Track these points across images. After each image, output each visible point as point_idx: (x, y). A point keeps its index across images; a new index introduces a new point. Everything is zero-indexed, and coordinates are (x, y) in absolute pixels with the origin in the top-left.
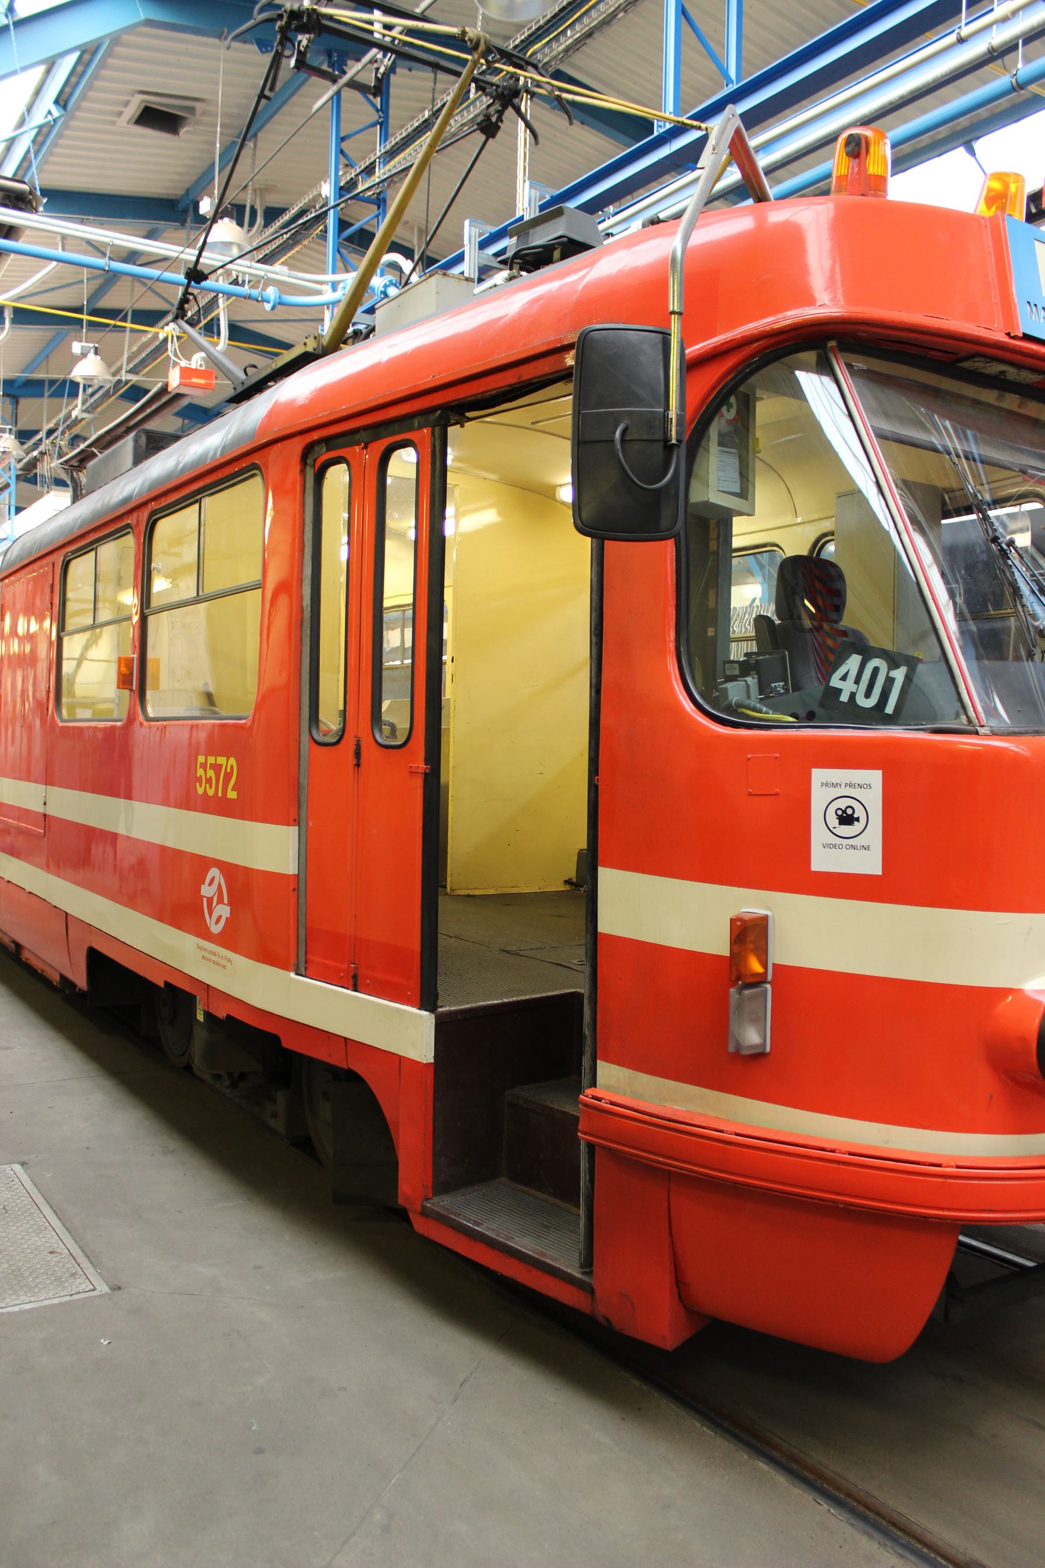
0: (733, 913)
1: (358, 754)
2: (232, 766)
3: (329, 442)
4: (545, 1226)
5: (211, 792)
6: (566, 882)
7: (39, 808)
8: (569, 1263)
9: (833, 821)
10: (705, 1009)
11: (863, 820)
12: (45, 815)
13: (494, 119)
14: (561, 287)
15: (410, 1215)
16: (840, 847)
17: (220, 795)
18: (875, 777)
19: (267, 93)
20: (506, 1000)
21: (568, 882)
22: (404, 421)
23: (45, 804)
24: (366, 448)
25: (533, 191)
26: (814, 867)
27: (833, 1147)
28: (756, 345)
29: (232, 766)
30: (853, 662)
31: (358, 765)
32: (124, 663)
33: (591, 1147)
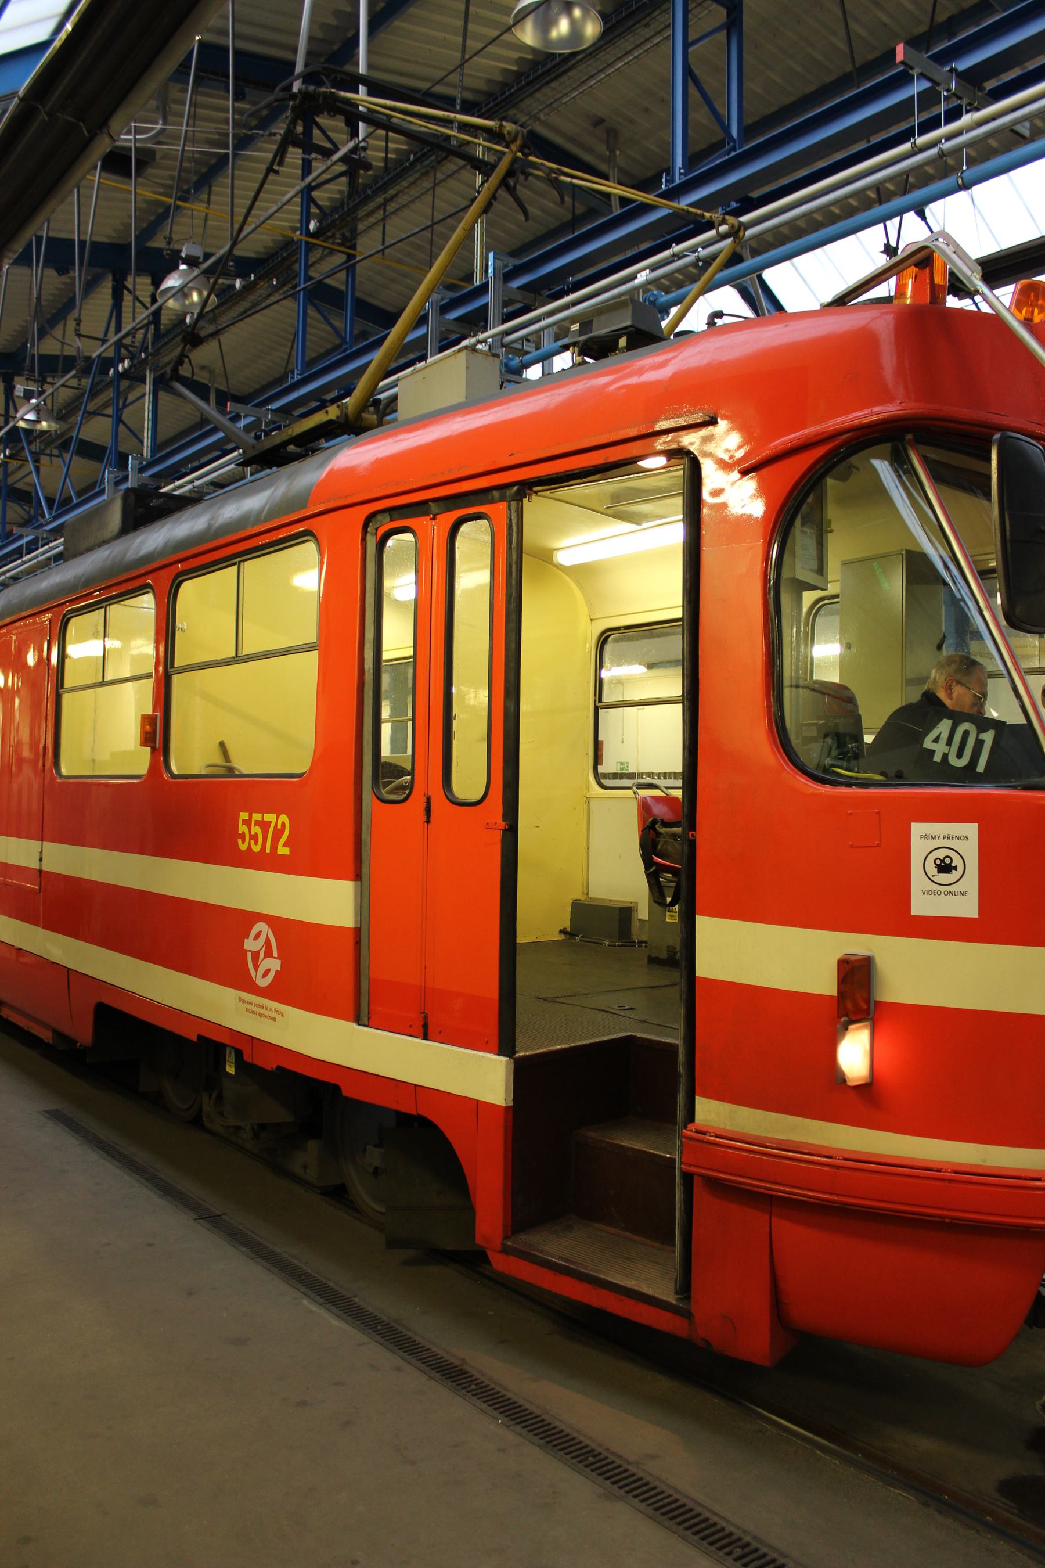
0: (839, 955)
1: (428, 811)
2: (283, 824)
3: (393, 512)
4: (627, 1259)
5: (256, 848)
6: (561, 931)
7: (36, 865)
8: (665, 1290)
9: (932, 870)
10: (784, 1046)
11: (960, 868)
12: (41, 871)
15: (489, 1253)
16: (939, 893)
17: (268, 850)
18: (971, 830)
20: (572, 1045)
21: (563, 932)
23: (41, 860)
24: (434, 519)
25: (498, 262)
26: (915, 912)
27: (939, 1167)
28: (844, 437)
29: (283, 824)
30: (944, 727)
31: (428, 822)
32: (148, 720)
33: (688, 1178)
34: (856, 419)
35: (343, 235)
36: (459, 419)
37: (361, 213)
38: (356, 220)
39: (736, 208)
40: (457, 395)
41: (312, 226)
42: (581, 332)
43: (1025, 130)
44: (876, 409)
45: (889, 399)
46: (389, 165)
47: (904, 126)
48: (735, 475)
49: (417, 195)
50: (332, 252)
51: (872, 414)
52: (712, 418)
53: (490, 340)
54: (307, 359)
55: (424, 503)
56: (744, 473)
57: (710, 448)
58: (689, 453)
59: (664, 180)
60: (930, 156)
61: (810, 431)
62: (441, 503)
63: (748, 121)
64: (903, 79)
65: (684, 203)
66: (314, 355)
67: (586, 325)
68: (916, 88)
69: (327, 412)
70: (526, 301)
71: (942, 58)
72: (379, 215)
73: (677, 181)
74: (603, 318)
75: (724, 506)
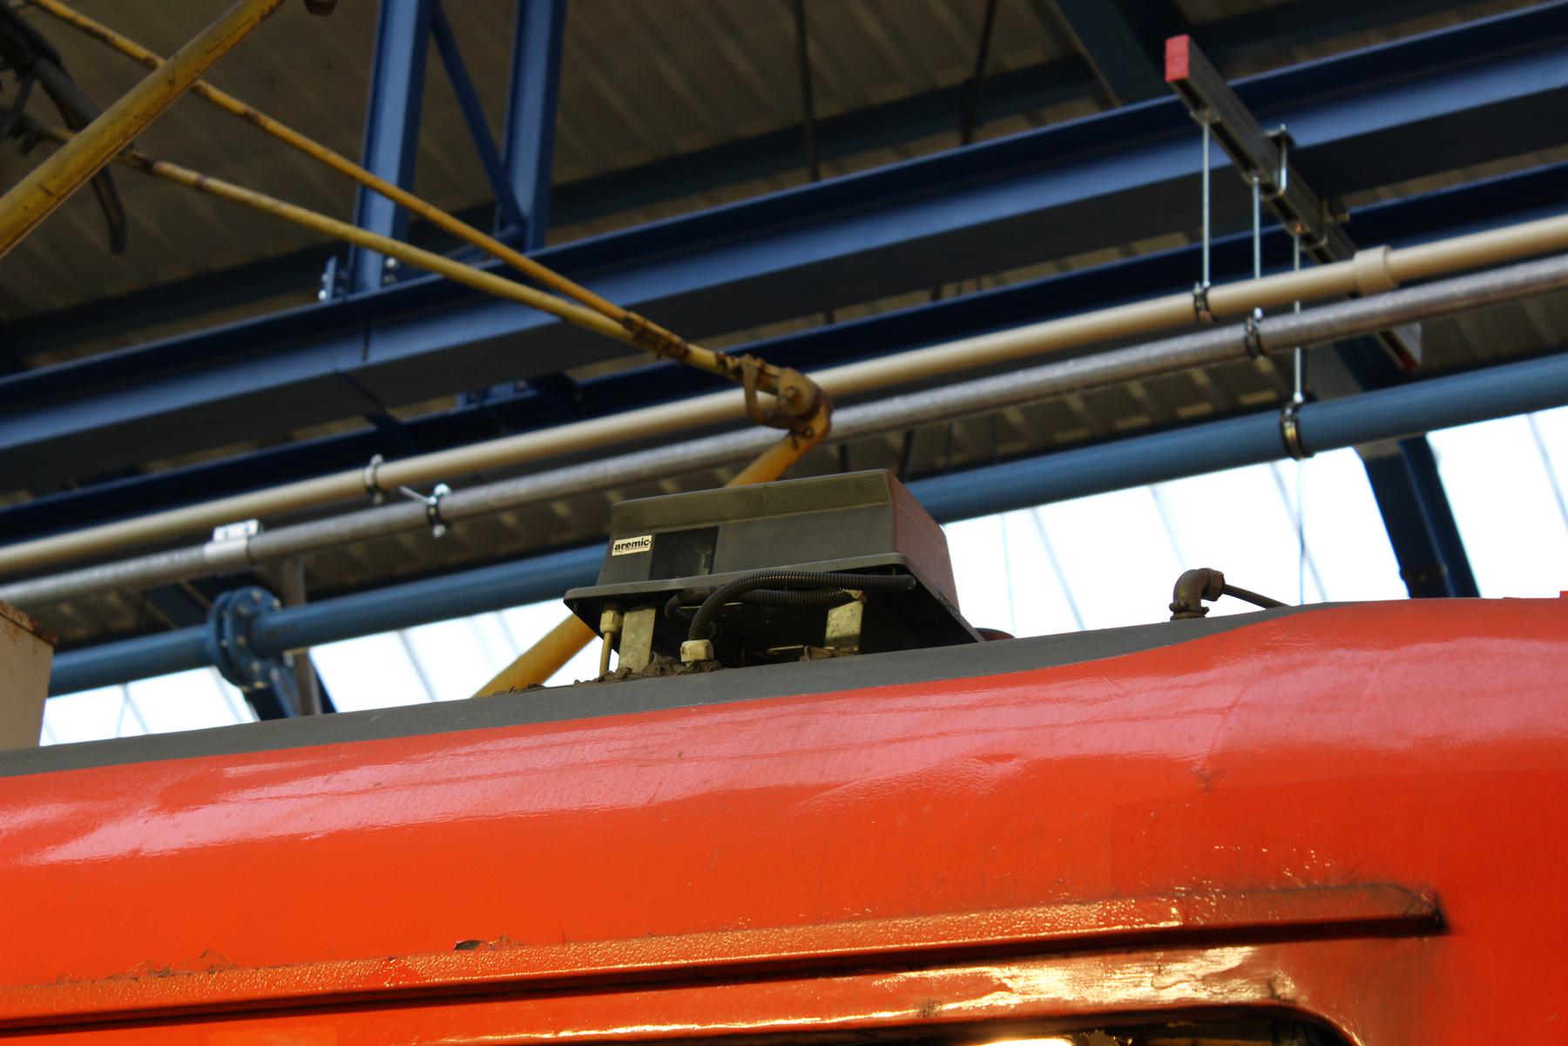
43: (1412, 340)
47: (1173, 244)
60: (1223, 346)
63: (563, 175)
64: (1170, 127)
68: (1207, 158)
71: (1269, 101)
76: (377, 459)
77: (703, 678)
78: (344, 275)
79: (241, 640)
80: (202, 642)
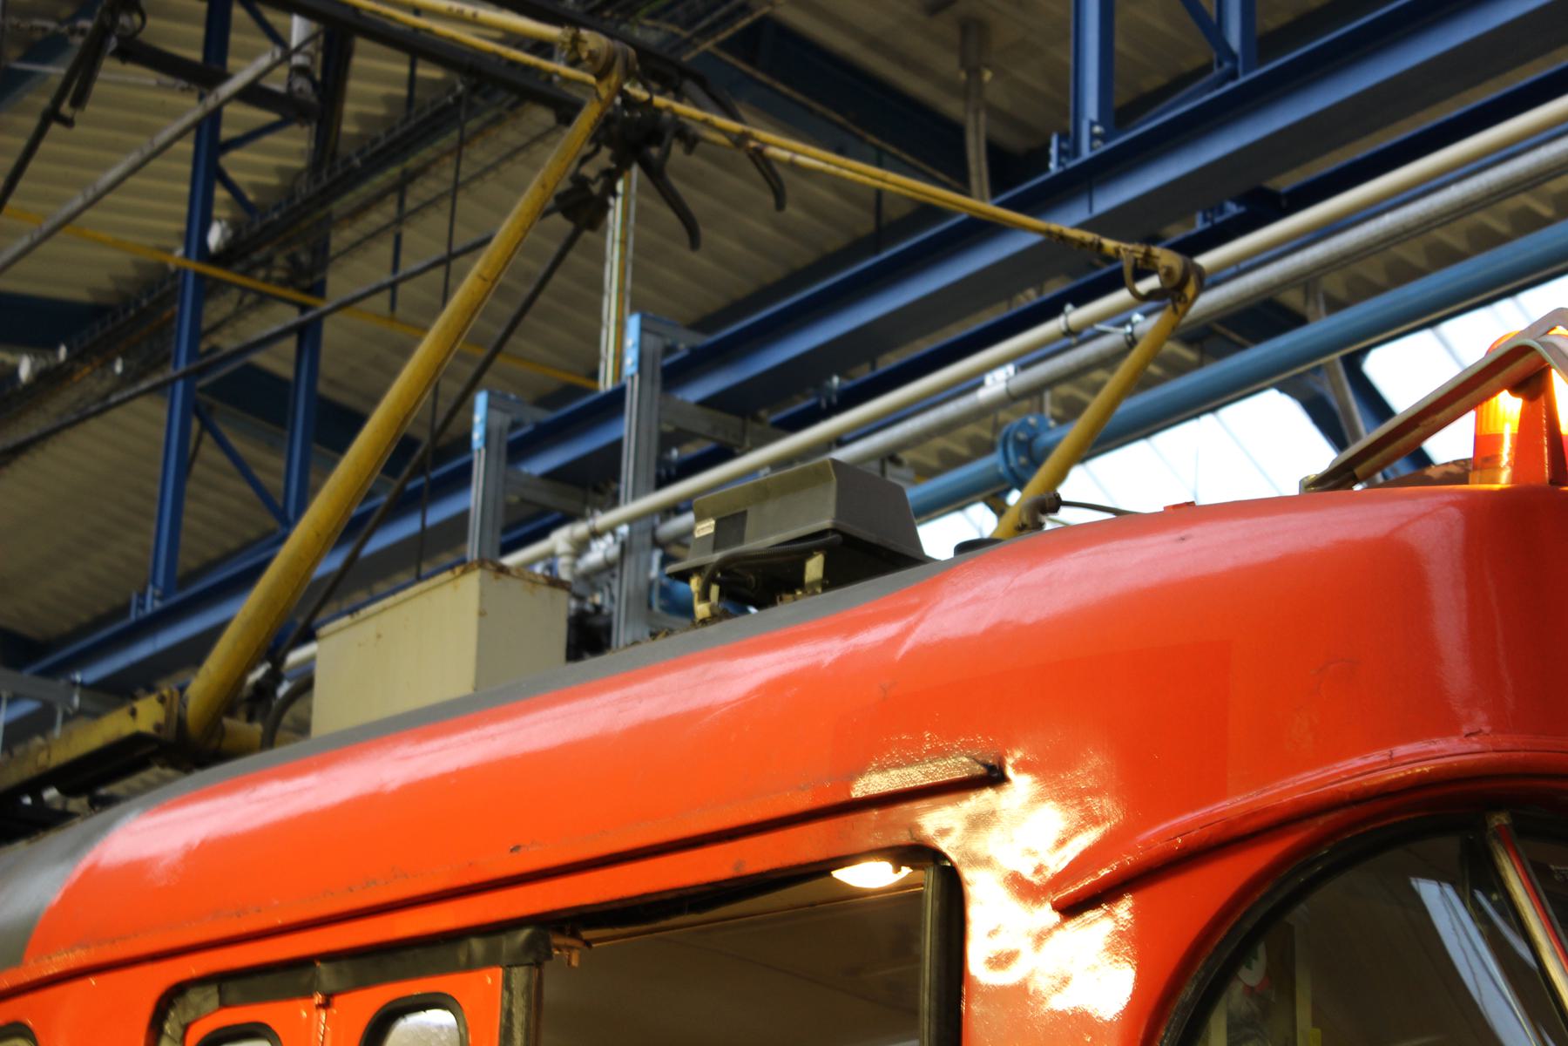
13: (596, 189)
14: (842, 661)
19: (65, 109)
22: (438, 949)
24: (326, 1005)
25: (651, 341)
28: (1321, 821)
34: (1351, 774)
35: (293, 259)
36: (404, 750)
37: (339, 206)
38: (329, 222)
39: (1237, 218)
40: (453, 675)
41: (215, 237)
42: (718, 540)
44: (1401, 750)
45: (1447, 725)
46: (418, 94)
48: (1046, 915)
49: (492, 160)
50: (263, 299)
51: (1393, 762)
52: (991, 768)
53: (624, 530)
54: (179, 572)
55: (303, 963)
56: (1071, 909)
57: (985, 843)
58: (937, 856)
59: (1053, 151)
61: (1234, 804)
62: (345, 966)
65: (1067, 222)
66: (193, 563)
67: (731, 525)
69: (133, 713)
70: (720, 436)
72: (390, 208)
73: (1086, 153)
74: (771, 507)
75: (1020, 992)
76: (1069, 307)
77: (712, 629)
78: (1064, 145)
79: (1023, 460)
80: (995, 466)
